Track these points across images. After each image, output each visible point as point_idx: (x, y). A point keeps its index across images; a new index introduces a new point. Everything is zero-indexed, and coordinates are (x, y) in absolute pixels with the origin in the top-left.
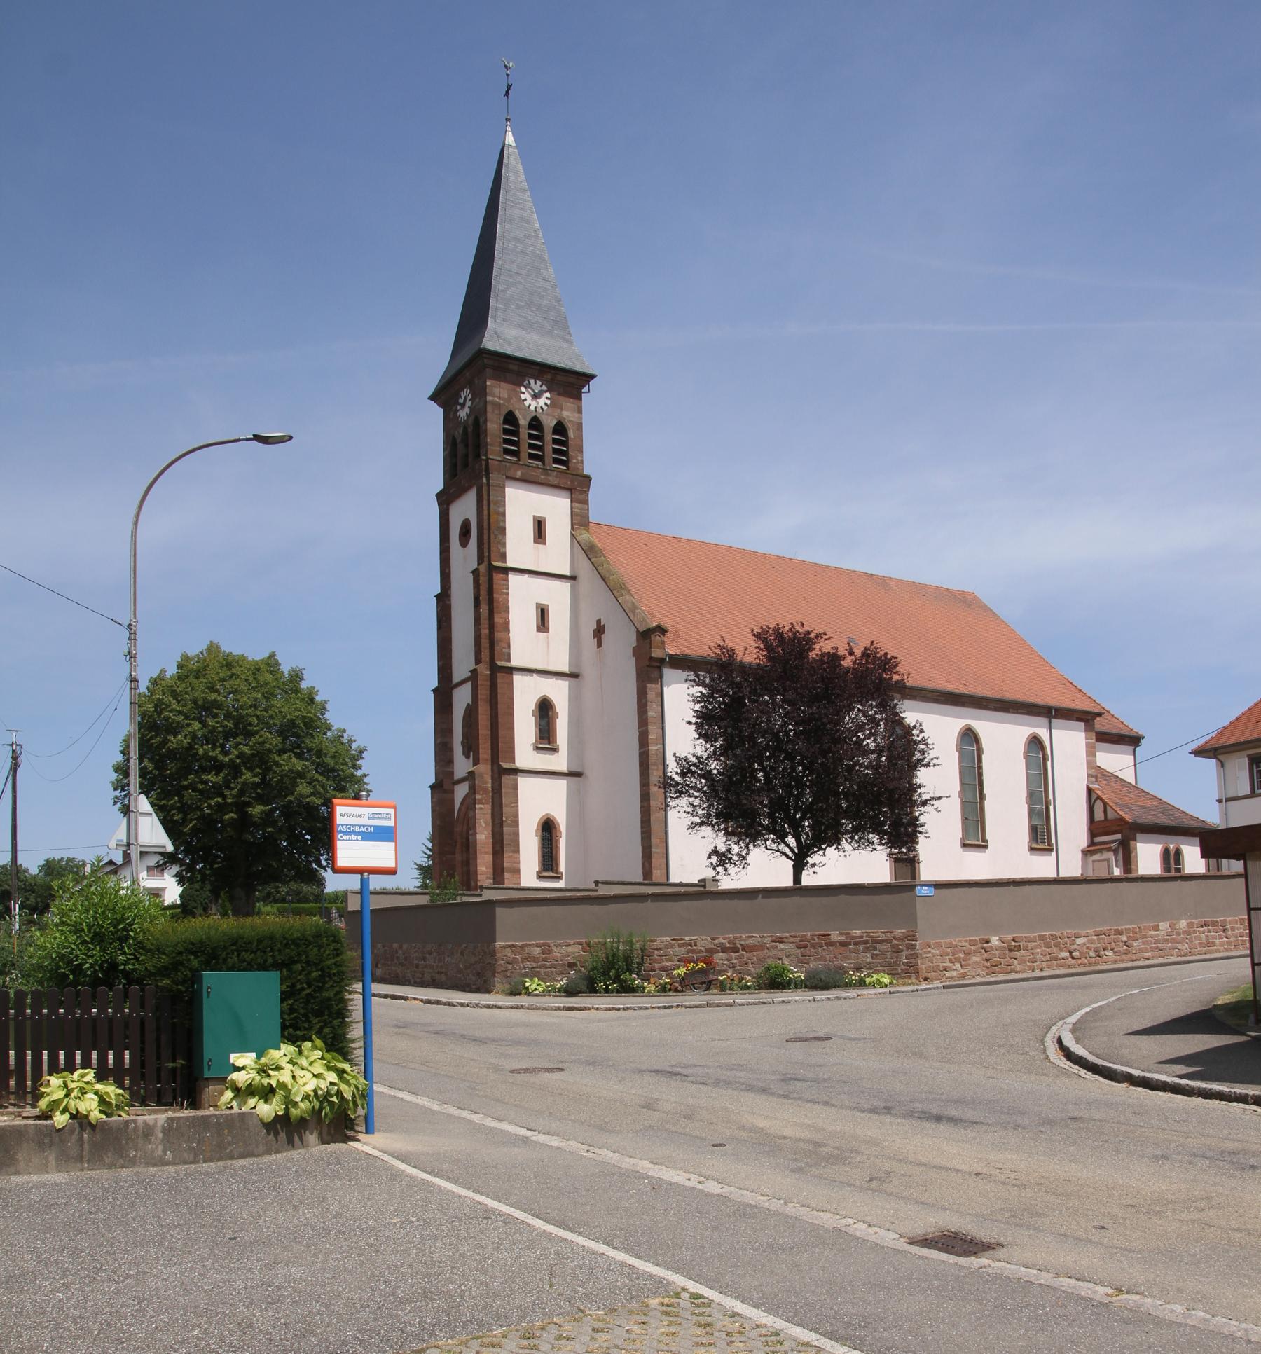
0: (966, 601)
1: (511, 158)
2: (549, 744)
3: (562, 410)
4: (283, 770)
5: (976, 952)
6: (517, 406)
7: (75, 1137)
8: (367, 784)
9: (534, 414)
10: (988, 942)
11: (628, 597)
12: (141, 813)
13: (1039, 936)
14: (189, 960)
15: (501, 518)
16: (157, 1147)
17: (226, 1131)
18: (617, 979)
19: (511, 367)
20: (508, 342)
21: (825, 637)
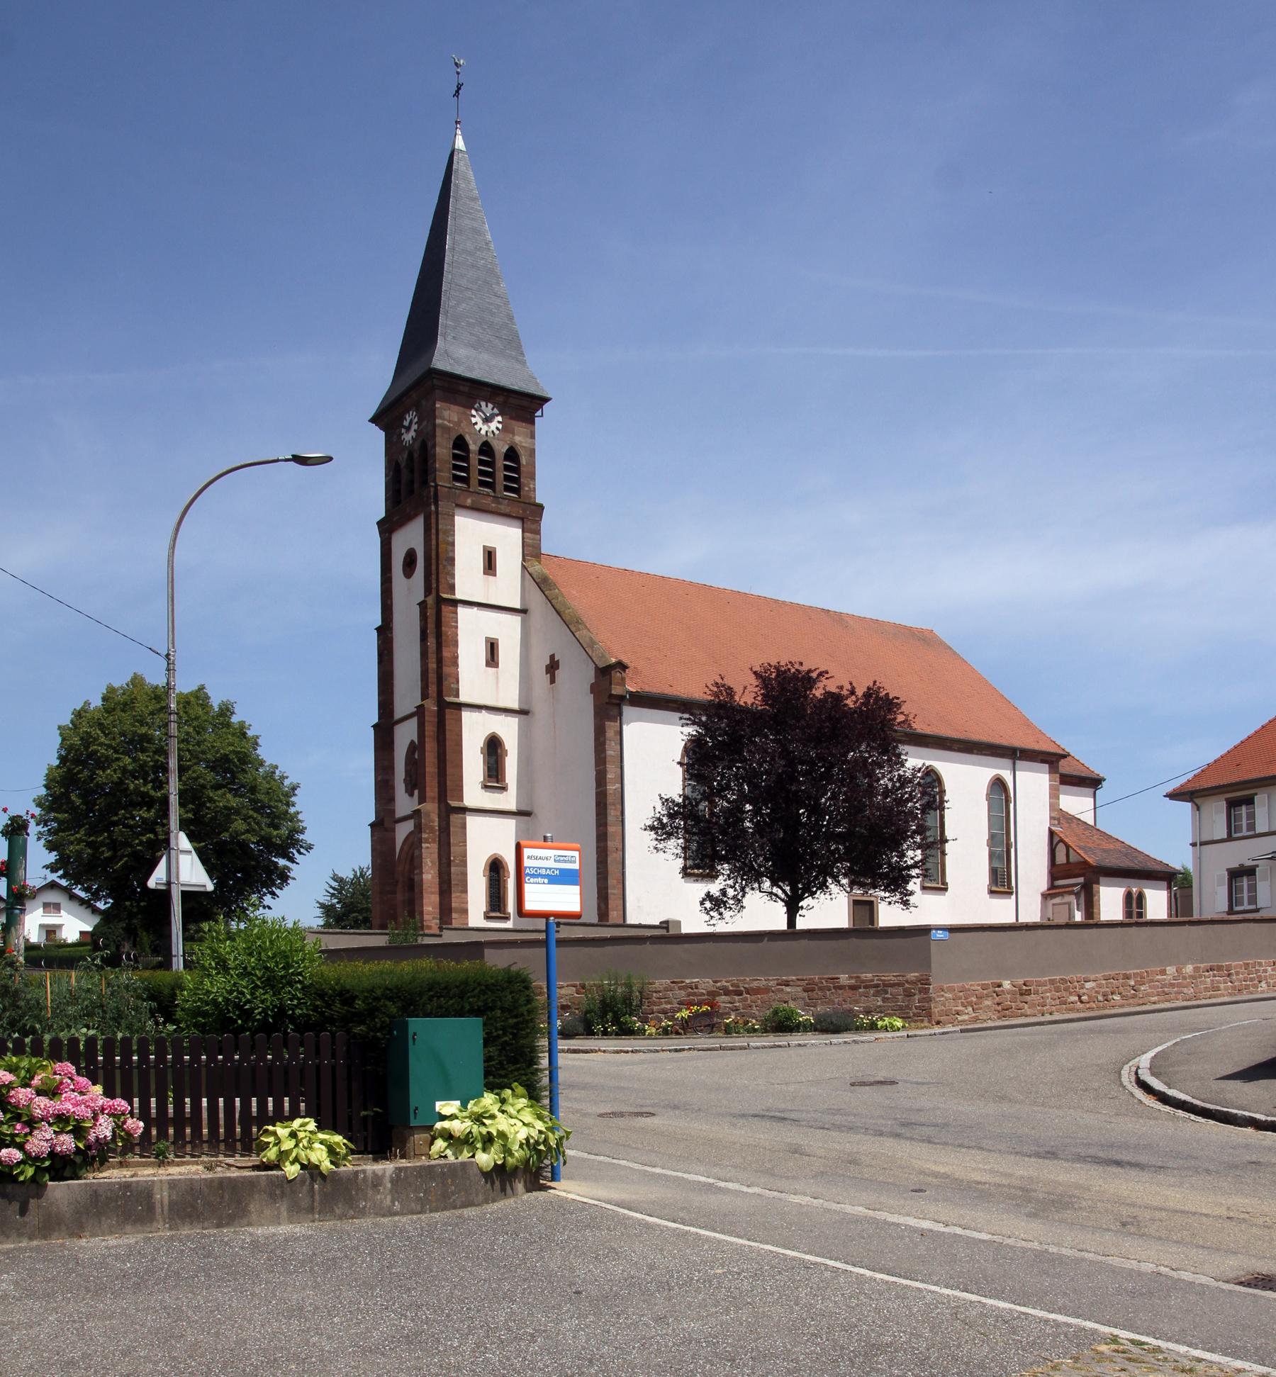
0: (923, 639)
1: (462, 163)
2: (498, 783)
3: (513, 434)
4: (217, 806)
5: (987, 996)
6: (467, 430)
7: (306, 1188)
8: (302, 821)
9: (485, 439)
10: (999, 986)
11: (585, 631)
12: (181, 851)
13: (1049, 980)
14: (386, 1006)
15: (450, 548)
16: (385, 1198)
17: (450, 1180)
18: (616, 1021)
19: (462, 388)
20: (458, 361)
21: (827, 676)
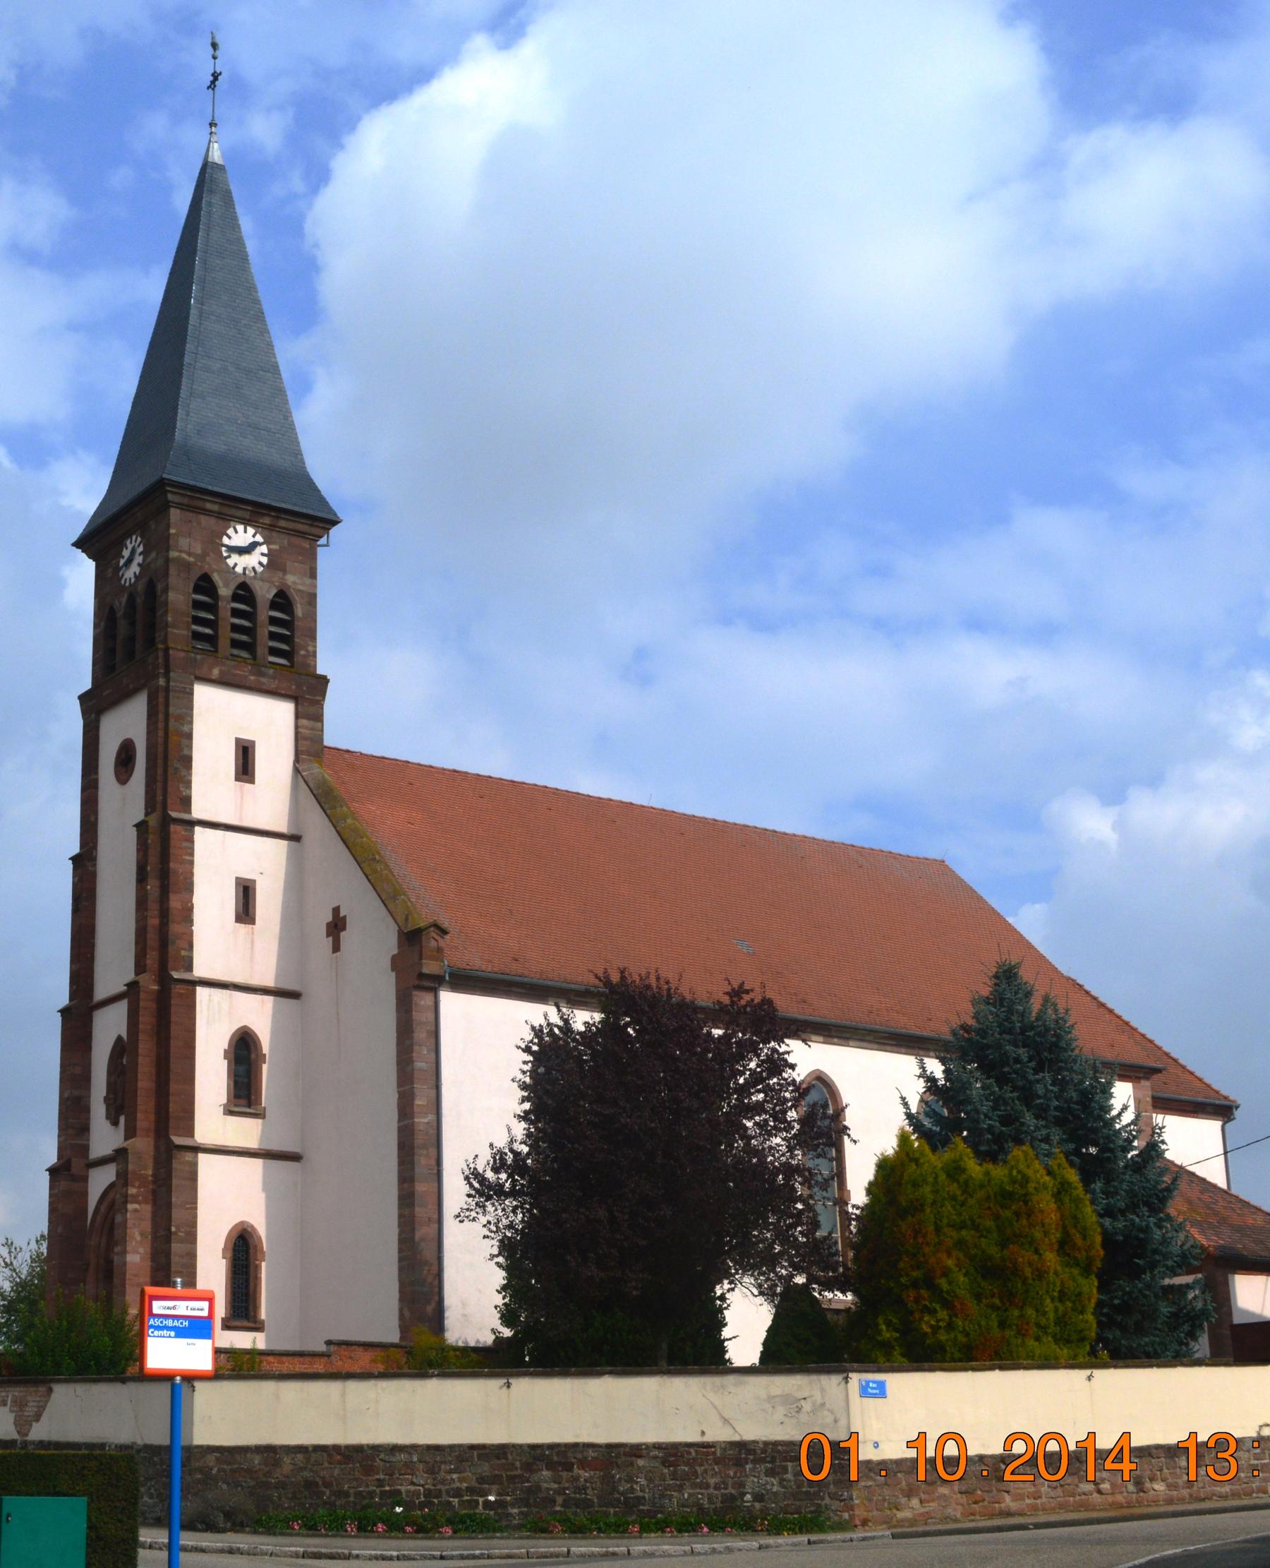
2: (249, 1106)
3: (285, 571)
6: (215, 567)
9: (242, 580)
19: (209, 506)
